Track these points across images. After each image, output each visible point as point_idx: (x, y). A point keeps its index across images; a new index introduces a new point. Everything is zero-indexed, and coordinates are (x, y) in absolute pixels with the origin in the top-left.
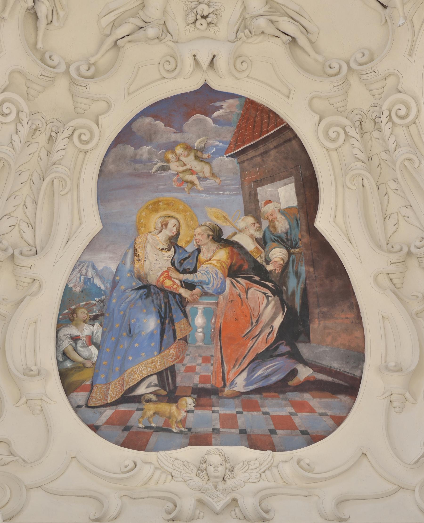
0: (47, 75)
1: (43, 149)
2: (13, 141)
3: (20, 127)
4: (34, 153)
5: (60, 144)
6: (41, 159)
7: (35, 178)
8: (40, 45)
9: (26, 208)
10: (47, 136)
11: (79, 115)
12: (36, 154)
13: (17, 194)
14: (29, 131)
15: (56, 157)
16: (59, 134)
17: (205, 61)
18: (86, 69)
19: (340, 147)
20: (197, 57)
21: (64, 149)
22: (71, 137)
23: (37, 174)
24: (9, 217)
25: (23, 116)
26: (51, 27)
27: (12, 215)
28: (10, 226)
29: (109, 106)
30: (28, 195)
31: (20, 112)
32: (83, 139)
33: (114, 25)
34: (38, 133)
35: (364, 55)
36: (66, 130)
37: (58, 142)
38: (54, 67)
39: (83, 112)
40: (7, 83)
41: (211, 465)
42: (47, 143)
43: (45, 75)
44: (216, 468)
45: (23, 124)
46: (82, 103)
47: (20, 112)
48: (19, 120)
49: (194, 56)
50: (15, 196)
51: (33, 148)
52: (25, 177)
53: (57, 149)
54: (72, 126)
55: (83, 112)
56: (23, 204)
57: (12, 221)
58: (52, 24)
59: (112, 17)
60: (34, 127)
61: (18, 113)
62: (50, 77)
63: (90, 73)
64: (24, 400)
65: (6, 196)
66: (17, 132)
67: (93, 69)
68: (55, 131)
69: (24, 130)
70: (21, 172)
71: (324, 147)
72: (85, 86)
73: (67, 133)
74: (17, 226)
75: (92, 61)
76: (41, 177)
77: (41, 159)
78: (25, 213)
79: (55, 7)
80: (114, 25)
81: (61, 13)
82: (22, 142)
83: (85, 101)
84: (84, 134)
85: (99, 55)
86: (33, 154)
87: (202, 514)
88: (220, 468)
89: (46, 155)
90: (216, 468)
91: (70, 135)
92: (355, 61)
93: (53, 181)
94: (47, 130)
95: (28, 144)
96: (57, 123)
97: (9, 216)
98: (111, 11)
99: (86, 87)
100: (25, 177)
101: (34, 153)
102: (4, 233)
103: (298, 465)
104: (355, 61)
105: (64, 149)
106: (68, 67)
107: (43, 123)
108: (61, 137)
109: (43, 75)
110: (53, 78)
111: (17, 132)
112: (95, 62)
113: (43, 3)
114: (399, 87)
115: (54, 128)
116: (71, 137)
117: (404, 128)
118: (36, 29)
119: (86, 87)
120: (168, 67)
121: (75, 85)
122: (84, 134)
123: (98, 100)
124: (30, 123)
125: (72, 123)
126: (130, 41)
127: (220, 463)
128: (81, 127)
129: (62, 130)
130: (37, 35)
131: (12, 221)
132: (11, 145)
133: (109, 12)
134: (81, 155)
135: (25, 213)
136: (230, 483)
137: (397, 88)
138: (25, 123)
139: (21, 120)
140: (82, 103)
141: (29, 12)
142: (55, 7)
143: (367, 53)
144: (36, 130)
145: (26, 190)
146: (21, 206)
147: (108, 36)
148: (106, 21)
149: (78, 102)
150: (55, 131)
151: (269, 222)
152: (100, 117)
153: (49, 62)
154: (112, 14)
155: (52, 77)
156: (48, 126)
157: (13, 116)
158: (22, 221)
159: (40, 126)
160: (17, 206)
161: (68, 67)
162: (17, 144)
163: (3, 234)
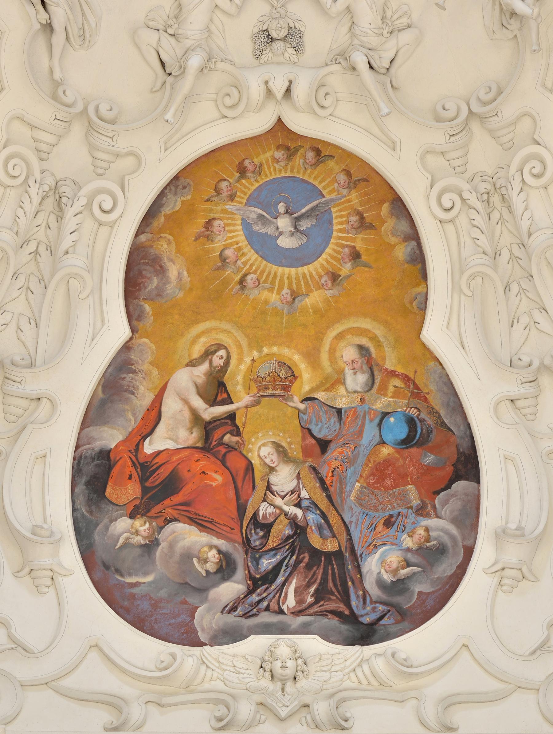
17: (279, 88)
19: (457, 216)
20: (271, 84)
22: (89, 206)
29: (139, 159)
35: (111, 110)
41: (277, 660)
44: (284, 664)
49: (267, 82)
64: (27, 570)
71: (435, 217)
73: (517, 185)
87: (263, 718)
88: (290, 664)
90: (284, 664)
92: (479, 99)
103: (393, 658)
104: (479, 99)
114: (536, 137)
117: (541, 190)
120: (228, 102)
125: (513, 169)
127: (289, 656)
134: (104, 231)
136: (302, 683)
137: (124, 176)
143: (115, 111)
151: (242, 177)
152: (127, 178)
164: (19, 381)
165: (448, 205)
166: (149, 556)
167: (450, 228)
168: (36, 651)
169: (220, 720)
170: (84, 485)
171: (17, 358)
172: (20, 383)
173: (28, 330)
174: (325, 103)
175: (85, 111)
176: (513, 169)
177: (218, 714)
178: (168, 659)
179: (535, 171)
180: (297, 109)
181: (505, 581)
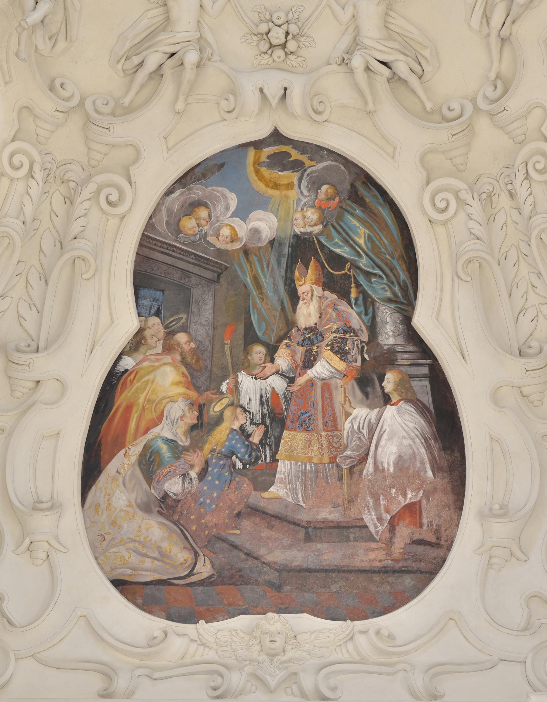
0: (458, 132)
1: (512, 210)
2: (472, 230)
3: (469, 210)
4: (506, 223)
5: (522, 193)
6: (516, 223)
7: (524, 248)
8: (429, 106)
9: (516, 287)
10: (507, 193)
11: (522, 143)
12: (509, 221)
13: (516, 280)
14: (482, 205)
15: (527, 209)
16: (513, 183)
18: (492, 90)
21: (531, 194)
22: (527, 177)
23: (523, 242)
24: (524, 312)
25: (466, 196)
26: (426, 77)
27: (526, 307)
28: (531, 320)
30: (529, 272)
31: (459, 193)
32: (540, 169)
33: (487, 18)
34: (495, 199)
36: (517, 173)
37: (518, 192)
38: (461, 116)
39: (523, 137)
40: (425, 173)
42: (512, 200)
43: (456, 133)
45: (470, 203)
46: (515, 130)
47: (459, 193)
48: (462, 203)
50: (516, 284)
51: (500, 219)
52: (513, 256)
53: (522, 202)
54: (520, 163)
55: (523, 137)
56: (530, 286)
57: (531, 314)
58: (425, 73)
59: (479, 12)
60: (484, 196)
61: (457, 197)
62: (464, 130)
63: (499, 91)
65: (505, 294)
66: (470, 217)
67: (499, 84)
68: (508, 182)
69: (476, 209)
70: (505, 253)
72: (504, 109)
73: (521, 176)
74: (540, 315)
75: (493, 76)
76: (42, 276)
77: (516, 223)
78: (539, 294)
79: (417, 53)
80: (487, 18)
81: (427, 53)
82: (482, 224)
83: (516, 124)
84: (538, 162)
85: (496, 64)
86: (504, 225)
89: (519, 215)
91: (525, 175)
93: (541, 238)
94: (502, 187)
95: (490, 219)
96: (507, 172)
97: (525, 311)
98: (473, 6)
99: (505, 109)
100: (513, 256)
101: (506, 223)
102: (530, 333)
105: (531, 194)
106: (475, 104)
107: (493, 185)
108: (517, 183)
109: (455, 134)
110: (470, 126)
111: (470, 217)
112: (497, 74)
113: (397, 60)
115: (506, 181)
116: (527, 177)
118: (413, 92)
119: (505, 109)
121: (495, 117)
122: (538, 162)
123: (529, 112)
124: (475, 196)
125: (519, 160)
126: (514, 22)
128: (531, 156)
129: (513, 176)
130: (419, 98)
131: (531, 314)
132: (472, 236)
133: (472, 9)
135: (539, 294)
138: (470, 201)
139: (465, 201)
140: (515, 130)
141: (394, 80)
142: (417, 53)
143: (112, 104)
144: (490, 197)
145: (524, 269)
146: (530, 289)
147: (488, 35)
148: (476, 20)
149: (511, 132)
150: (508, 182)
153: (450, 115)
154: (477, 8)
155: (467, 128)
156: (500, 181)
157: (453, 204)
158: (541, 306)
159: (491, 189)
160: (525, 294)
161: (475, 104)
162: (478, 230)
163: (529, 335)
164: (27, 363)
165: (443, 205)
166: (353, 377)
167: (440, 230)
168: (18, 625)
169: (215, 689)
170: (197, 474)
171: (23, 345)
172: (28, 365)
173: (30, 316)
174: (320, 109)
175: (81, 103)
176: (519, 160)
177: (212, 684)
178: (158, 634)
179: (539, 167)
180: (293, 116)
181: (494, 560)
